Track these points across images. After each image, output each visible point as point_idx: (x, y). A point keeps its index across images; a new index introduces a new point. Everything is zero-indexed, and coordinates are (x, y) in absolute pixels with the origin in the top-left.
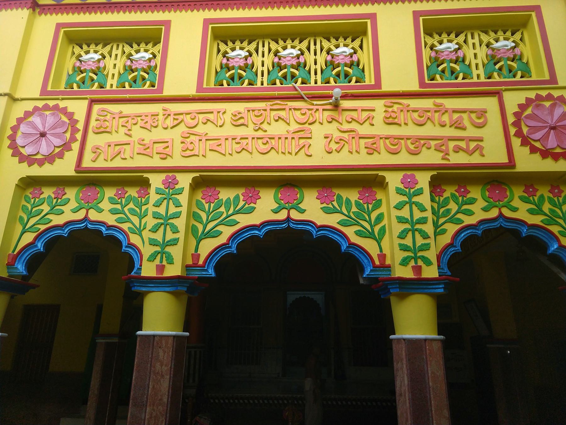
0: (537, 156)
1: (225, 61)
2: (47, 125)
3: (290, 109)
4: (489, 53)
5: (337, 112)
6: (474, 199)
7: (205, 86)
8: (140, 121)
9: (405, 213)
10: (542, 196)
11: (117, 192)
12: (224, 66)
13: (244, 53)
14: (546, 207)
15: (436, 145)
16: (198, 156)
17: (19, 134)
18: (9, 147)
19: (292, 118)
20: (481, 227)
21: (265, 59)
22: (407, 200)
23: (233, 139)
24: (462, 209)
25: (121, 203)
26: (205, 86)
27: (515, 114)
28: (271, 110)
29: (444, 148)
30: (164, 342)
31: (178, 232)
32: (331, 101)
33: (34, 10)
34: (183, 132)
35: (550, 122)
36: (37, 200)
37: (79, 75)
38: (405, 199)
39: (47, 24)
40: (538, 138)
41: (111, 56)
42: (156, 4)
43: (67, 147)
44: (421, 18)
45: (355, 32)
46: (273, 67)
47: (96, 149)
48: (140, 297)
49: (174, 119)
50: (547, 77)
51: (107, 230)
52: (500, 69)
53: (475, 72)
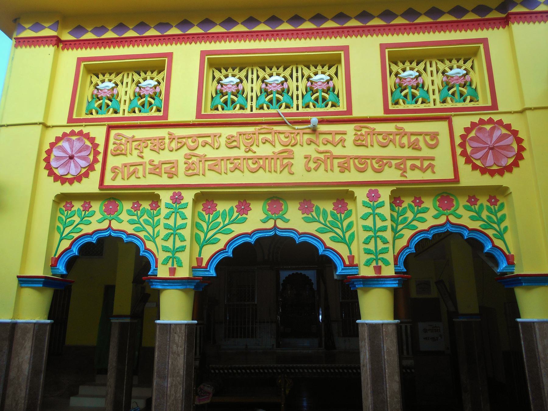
0: (478, 172)
1: (219, 87)
2: (74, 149)
3: (275, 133)
4: (444, 80)
5: (315, 135)
6: (427, 208)
7: (203, 113)
8: (150, 145)
9: (369, 223)
10: (481, 205)
11: (133, 205)
12: (218, 92)
13: (236, 80)
14: (485, 214)
15: (396, 164)
16: (199, 175)
17: (52, 157)
18: (45, 168)
19: (277, 142)
20: (432, 232)
21: (254, 85)
22: (371, 211)
23: (227, 160)
24: (417, 216)
25: (137, 215)
26: (203, 113)
27: (462, 137)
28: (259, 133)
29: (402, 166)
30: (178, 329)
31: (185, 240)
32: (310, 126)
33: (58, 46)
34: (186, 155)
35: (489, 143)
36: (69, 212)
37: (97, 102)
38: (370, 211)
39: (70, 57)
40: (479, 157)
41: (122, 84)
42: (160, 38)
43: (91, 168)
44: (387, 50)
45: (330, 61)
46: (261, 93)
47: (114, 169)
48: (158, 292)
49: (178, 142)
50: (490, 104)
51: (127, 237)
52: (453, 94)
53: (432, 97)
